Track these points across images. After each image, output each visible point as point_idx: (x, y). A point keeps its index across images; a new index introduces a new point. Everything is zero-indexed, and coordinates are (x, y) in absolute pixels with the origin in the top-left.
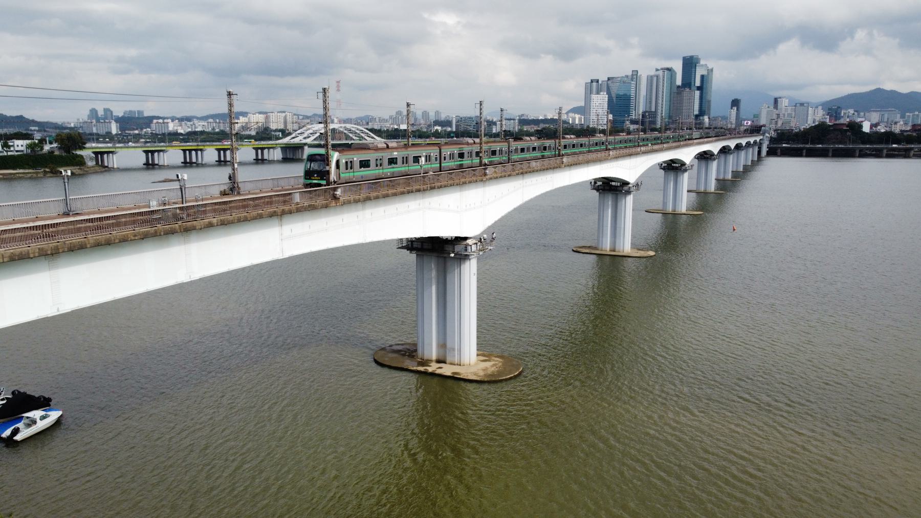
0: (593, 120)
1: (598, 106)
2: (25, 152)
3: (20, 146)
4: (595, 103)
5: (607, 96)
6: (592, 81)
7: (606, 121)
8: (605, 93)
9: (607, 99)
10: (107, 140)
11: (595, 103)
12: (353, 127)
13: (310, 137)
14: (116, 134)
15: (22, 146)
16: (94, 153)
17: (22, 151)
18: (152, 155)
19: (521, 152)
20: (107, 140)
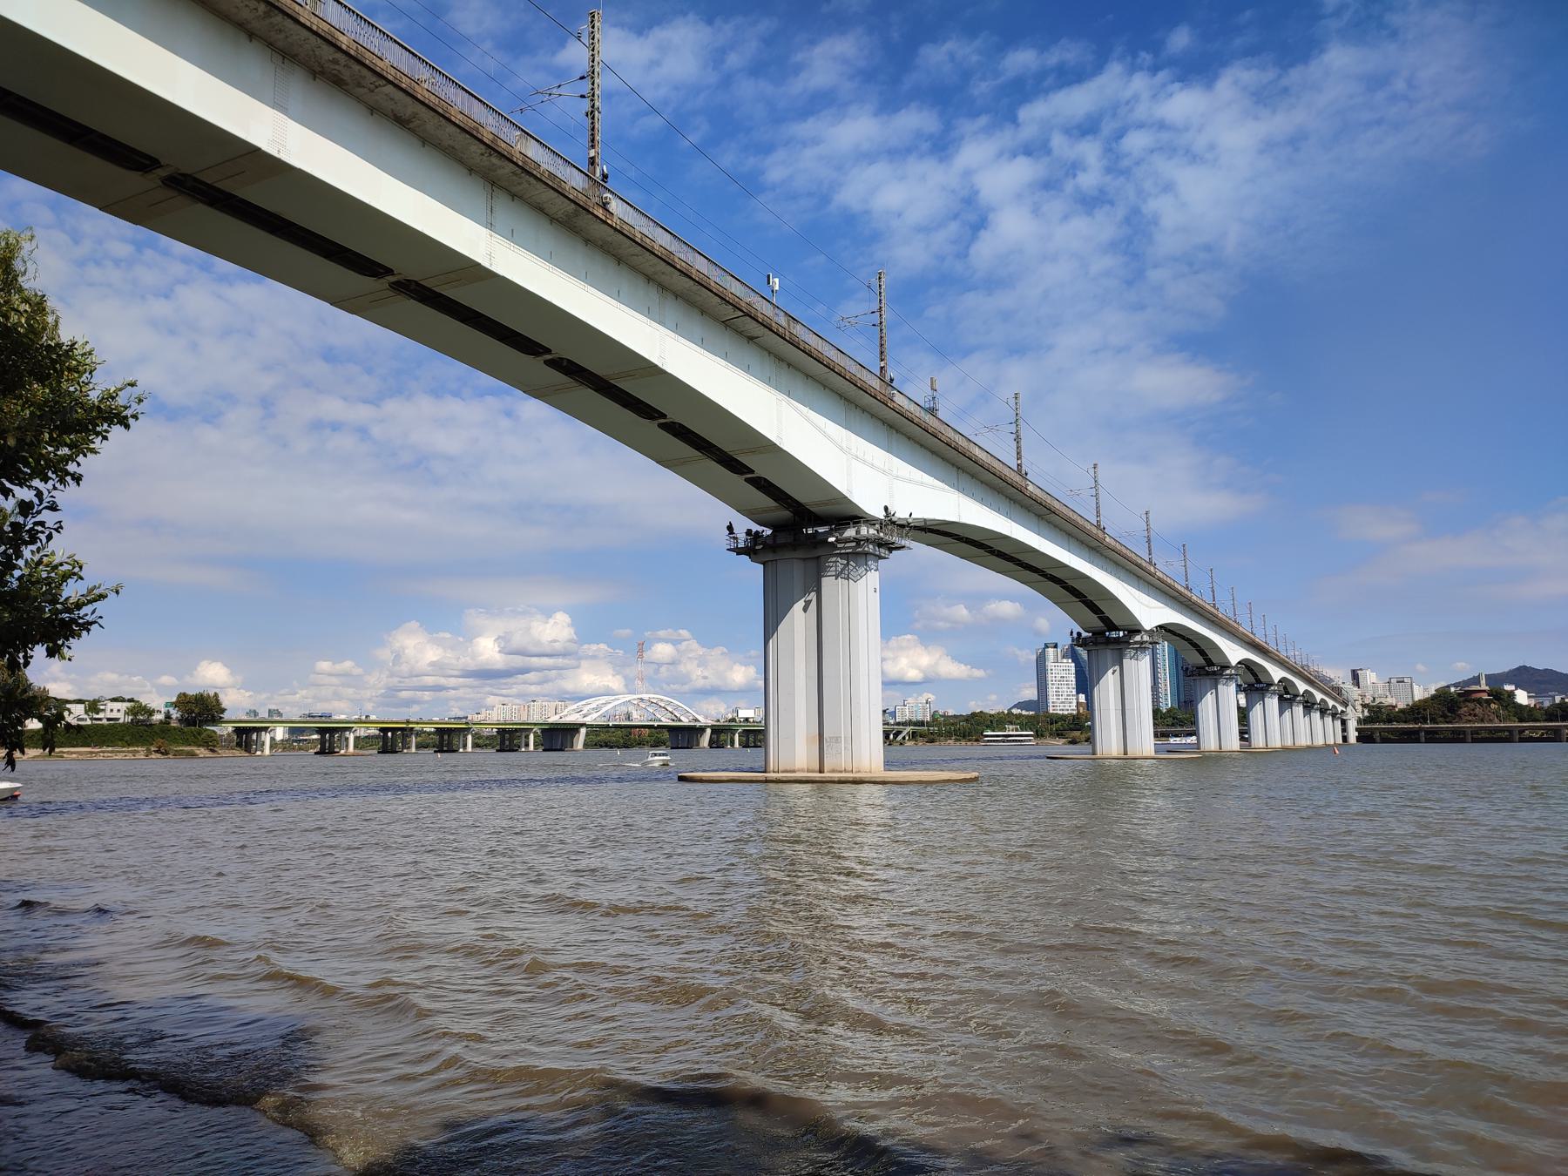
0: (1053, 702)
1: (1059, 681)
2: (121, 721)
3: (115, 711)
4: (1054, 675)
5: (1073, 665)
6: (1046, 646)
7: (1075, 704)
8: (1070, 661)
9: (1073, 670)
10: (42, 463)
11: (1054, 675)
12: (662, 700)
13: (590, 714)
14: (282, 740)
15: (119, 711)
16: (382, 730)
17: (118, 719)
18: (332, 736)
19: (745, 745)
20: (42, 463)
